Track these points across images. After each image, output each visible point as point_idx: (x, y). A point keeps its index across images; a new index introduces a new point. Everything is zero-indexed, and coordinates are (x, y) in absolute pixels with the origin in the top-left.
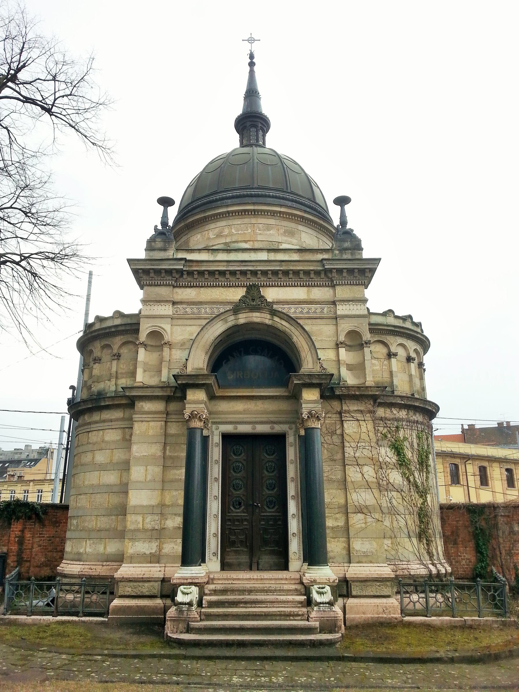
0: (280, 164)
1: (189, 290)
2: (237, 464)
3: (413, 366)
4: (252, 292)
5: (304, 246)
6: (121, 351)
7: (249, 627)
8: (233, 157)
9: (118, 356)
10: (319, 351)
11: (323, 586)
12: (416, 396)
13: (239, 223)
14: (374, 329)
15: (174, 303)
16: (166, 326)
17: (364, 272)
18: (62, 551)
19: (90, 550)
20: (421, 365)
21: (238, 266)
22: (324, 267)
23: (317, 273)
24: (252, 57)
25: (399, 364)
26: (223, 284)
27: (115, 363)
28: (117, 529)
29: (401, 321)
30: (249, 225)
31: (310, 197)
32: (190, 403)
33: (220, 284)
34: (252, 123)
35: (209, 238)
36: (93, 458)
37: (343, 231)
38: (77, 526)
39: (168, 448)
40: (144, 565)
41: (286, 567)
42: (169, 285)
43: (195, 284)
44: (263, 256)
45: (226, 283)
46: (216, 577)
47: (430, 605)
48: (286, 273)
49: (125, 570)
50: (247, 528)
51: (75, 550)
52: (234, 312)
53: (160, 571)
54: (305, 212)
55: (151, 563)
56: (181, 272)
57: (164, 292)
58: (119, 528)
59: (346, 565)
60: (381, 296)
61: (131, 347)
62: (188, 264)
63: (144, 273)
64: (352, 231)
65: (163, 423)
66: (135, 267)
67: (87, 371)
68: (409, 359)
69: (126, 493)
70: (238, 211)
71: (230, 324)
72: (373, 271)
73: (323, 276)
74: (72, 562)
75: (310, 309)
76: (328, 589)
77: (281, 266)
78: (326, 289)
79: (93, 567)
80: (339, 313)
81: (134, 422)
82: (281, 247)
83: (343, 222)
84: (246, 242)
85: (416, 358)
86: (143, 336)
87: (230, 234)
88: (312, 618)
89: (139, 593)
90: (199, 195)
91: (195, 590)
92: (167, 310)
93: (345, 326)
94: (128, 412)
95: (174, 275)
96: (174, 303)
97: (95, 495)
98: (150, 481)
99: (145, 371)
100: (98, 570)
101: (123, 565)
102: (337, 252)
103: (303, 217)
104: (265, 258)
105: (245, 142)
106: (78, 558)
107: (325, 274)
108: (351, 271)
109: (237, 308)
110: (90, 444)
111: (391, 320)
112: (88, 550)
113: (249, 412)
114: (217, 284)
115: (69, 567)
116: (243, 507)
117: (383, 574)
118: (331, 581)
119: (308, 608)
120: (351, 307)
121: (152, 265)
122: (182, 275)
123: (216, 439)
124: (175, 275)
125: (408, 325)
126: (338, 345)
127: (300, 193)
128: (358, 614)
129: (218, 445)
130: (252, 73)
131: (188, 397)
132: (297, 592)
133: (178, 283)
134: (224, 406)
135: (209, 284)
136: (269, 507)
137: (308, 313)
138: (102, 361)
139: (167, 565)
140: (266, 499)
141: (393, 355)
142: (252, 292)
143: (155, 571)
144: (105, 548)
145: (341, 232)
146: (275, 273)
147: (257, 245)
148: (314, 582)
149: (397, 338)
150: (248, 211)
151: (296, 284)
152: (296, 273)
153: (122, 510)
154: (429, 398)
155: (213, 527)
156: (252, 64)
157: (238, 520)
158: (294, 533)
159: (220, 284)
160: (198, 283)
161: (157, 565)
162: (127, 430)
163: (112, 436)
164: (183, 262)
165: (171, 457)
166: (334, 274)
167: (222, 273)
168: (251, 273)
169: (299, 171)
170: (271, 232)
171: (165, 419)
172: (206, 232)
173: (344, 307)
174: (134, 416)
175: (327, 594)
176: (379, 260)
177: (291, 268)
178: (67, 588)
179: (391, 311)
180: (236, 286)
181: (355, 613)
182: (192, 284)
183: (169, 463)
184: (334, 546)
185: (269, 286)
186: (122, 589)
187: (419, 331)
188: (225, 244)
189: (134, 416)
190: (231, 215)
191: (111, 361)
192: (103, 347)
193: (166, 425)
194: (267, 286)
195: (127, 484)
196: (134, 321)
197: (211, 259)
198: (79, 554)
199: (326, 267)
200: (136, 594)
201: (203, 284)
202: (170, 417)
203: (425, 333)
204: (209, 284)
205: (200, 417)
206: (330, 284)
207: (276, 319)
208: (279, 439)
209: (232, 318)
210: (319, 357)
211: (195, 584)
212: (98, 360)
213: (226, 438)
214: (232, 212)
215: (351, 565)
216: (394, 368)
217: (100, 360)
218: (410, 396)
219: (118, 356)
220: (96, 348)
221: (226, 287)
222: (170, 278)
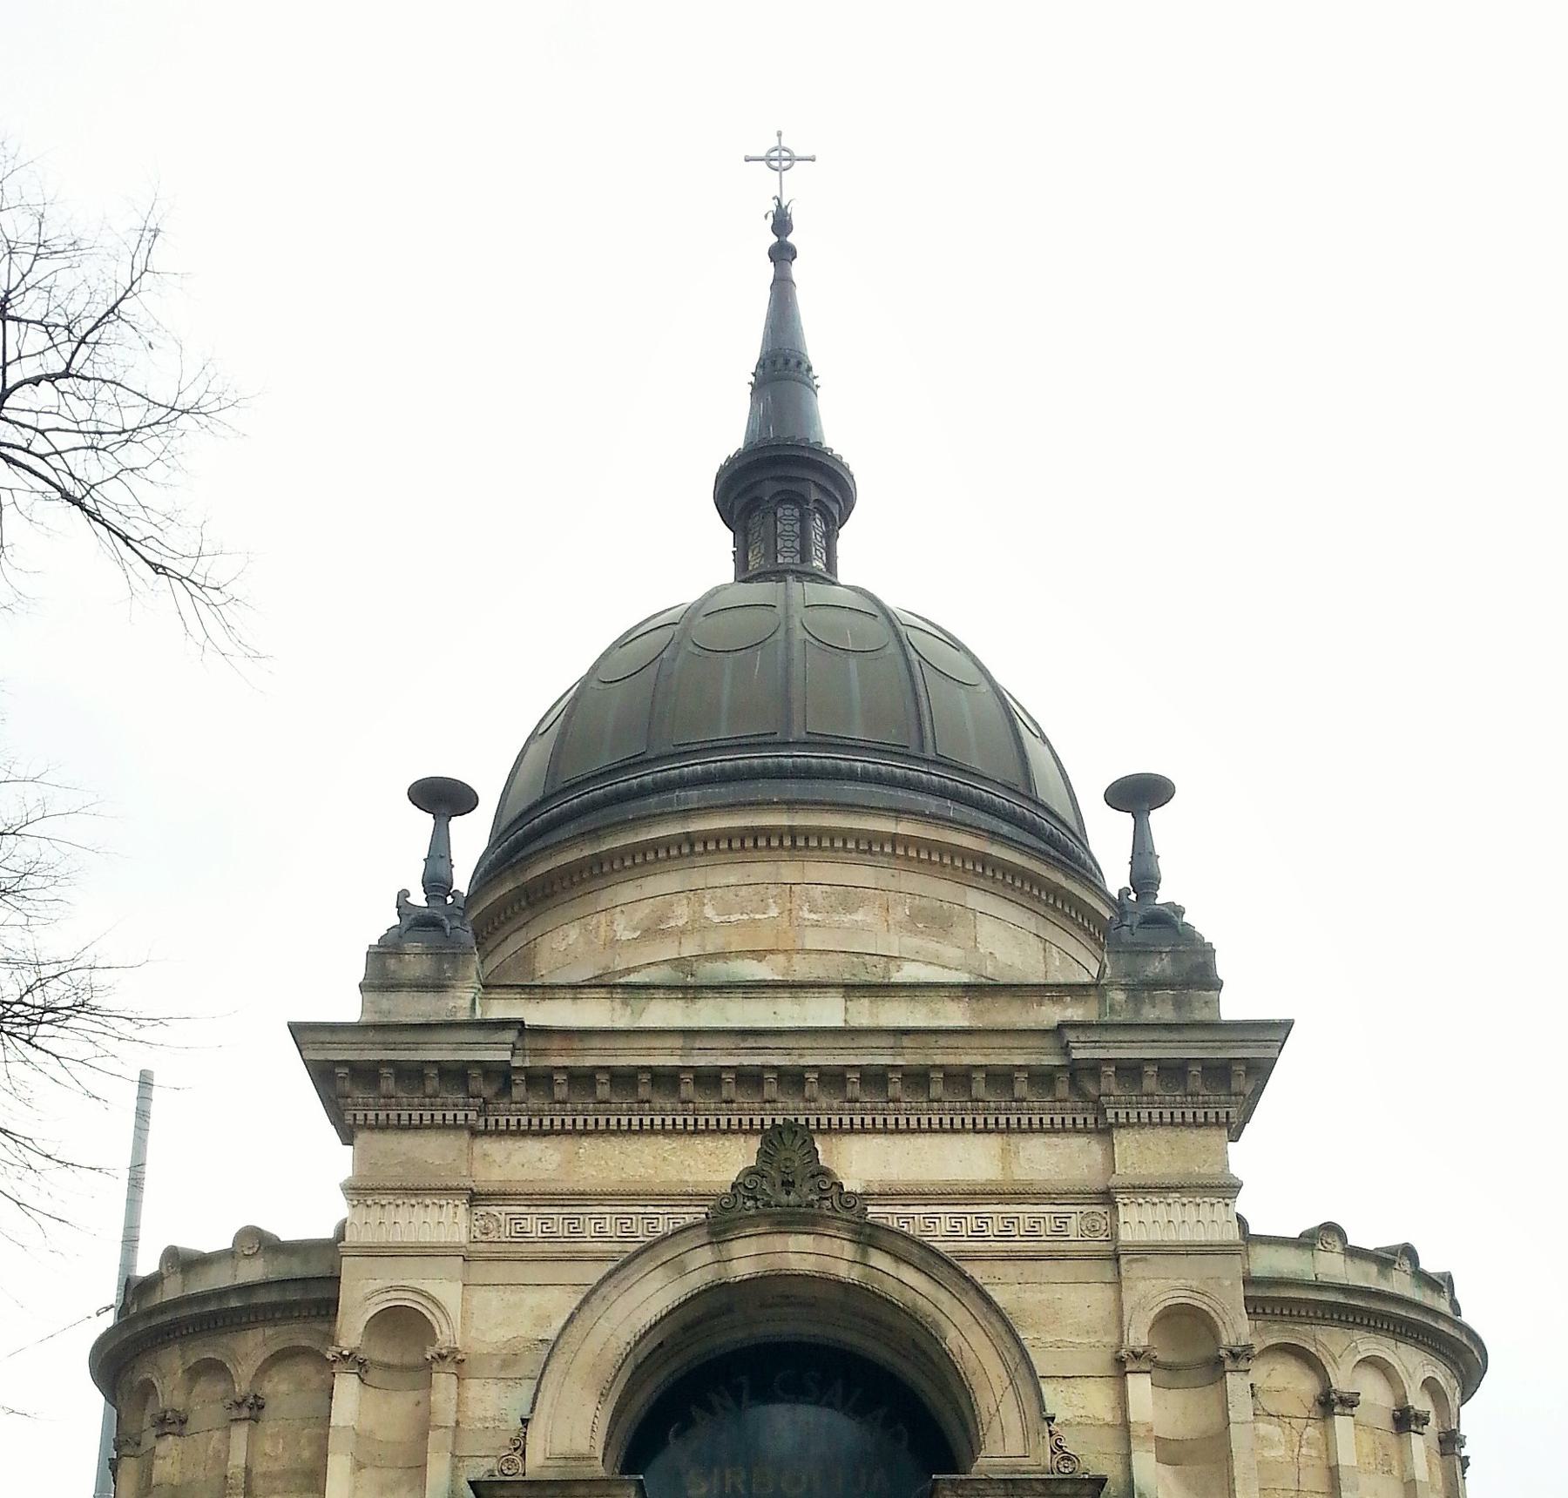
0: (893, 648)
3: (1420, 1446)
4: (784, 1154)
5: (990, 970)
6: (267, 1388)
7: (1042, 796)
8: (710, 620)
9: (253, 1408)
13: (732, 880)
14: (1266, 1300)
15: (475, 1198)
16: (444, 1289)
20: (1450, 1442)
22: (1068, 1054)
23: (1041, 1078)
24: (782, 223)
25: (1367, 1440)
26: (669, 1121)
27: (240, 1433)
29: (1373, 1269)
30: (773, 890)
31: (1014, 777)
34: (781, 487)
35: (613, 943)
42: (456, 1127)
44: (827, 1012)
48: (917, 1078)
52: (712, 1234)
54: (994, 836)
56: (501, 1075)
57: (434, 1152)
60: (1291, 1171)
61: (306, 1369)
62: (528, 1042)
64: (1180, 911)
66: (320, 1056)
67: (129, 1466)
68: (1405, 1420)
71: (697, 1280)
72: (1260, 1071)
73: (1062, 1089)
75: (1012, 1221)
77: (897, 1050)
78: (1078, 1142)
80: (1126, 1235)
82: (897, 977)
83: (1144, 876)
84: (759, 955)
85: (1432, 1417)
86: (351, 1329)
87: (698, 926)
90: (572, 773)
92: (448, 1224)
93: (1153, 1290)
96: (475, 1198)
99: (359, 1466)
102: (1120, 996)
103: (983, 859)
105: (754, 563)
107: (1074, 1083)
108: (1174, 1072)
109: (723, 1219)
111: (1331, 1266)
120: (1176, 1213)
121: (387, 1047)
122: (506, 1088)
124: (477, 1085)
125: (1399, 1283)
126: (1121, 1366)
127: (975, 764)
130: (782, 289)
135: (613, 1121)
137: (1004, 1236)
138: (192, 1425)
141: (1235, 1356)
142: (784, 1154)
145: (1137, 919)
147: (803, 970)
149: (1358, 1334)
150: (767, 832)
151: (958, 1121)
152: (959, 1078)
156: (782, 254)
160: (568, 1120)
164: (510, 1036)
167: (666, 1079)
168: (779, 1080)
169: (971, 676)
170: (859, 916)
172: (603, 917)
173: (1148, 1213)
176: (1286, 1026)
177: (939, 1059)
179: (1331, 1229)
182: (546, 1122)
188: (678, 963)
191: (228, 1428)
192: (197, 1372)
196: (316, 1269)
197: (622, 1023)
199: (1076, 1055)
201: (591, 1120)
204: (613, 1121)
206: (1091, 1120)
207: (879, 1260)
209: (706, 1255)
210: (1049, 1411)
214: (705, 838)
216: (1346, 1456)
217: (183, 1422)
219: (253, 1408)
220: (168, 1376)
221: (680, 1133)
222: (459, 1097)
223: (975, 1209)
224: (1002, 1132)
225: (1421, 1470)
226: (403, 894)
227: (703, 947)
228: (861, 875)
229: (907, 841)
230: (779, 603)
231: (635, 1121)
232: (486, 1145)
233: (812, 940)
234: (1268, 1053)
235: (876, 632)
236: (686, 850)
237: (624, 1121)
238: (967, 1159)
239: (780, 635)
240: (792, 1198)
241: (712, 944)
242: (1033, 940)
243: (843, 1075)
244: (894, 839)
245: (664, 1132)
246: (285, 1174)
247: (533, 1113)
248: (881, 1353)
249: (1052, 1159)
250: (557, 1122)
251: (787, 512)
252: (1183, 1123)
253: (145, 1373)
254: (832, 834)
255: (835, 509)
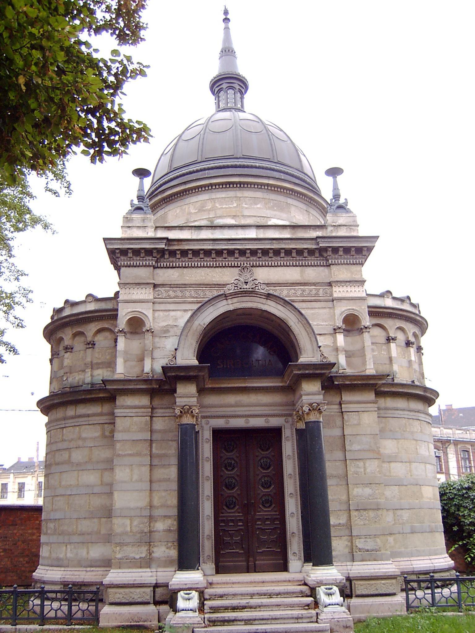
0: (264, 131)
1: (170, 271)
2: (229, 461)
3: (412, 350)
4: (246, 274)
5: (294, 221)
6: (96, 339)
7: (305, 172)
9: (92, 345)
10: (318, 337)
11: (330, 587)
12: (417, 383)
13: (223, 196)
14: (375, 312)
16: (147, 311)
17: (357, 250)
18: (38, 556)
19: (71, 555)
20: (419, 349)
21: (225, 245)
22: (318, 245)
23: (311, 252)
24: (226, 12)
25: (399, 349)
26: (208, 264)
27: (89, 351)
28: (100, 533)
29: (400, 302)
30: (235, 199)
31: (299, 167)
32: (180, 397)
33: (205, 264)
34: (229, 84)
35: (190, 213)
36: (70, 457)
37: (337, 205)
38: (55, 530)
39: (154, 445)
40: (134, 570)
41: (284, 568)
42: (149, 266)
43: (177, 264)
44: (252, 234)
45: (211, 264)
46: (214, 582)
47: (436, 602)
48: (277, 252)
49: (114, 576)
50: (242, 529)
51: (54, 555)
53: (152, 576)
54: (295, 184)
55: (141, 567)
56: (162, 252)
57: (143, 273)
58: (103, 531)
59: (348, 563)
60: (378, 277)
61: (107, 334)
63: (120, 254)
65: (148, 418)
66: (111, 247)
67: (55, 361)
68: (408, 344)
69: (110, 494)
70: (222, 184)
72: (370, 249)
74: (51, 568)
75: (304, 291)
76: (336, 589)
78: (322, 268)
79: (76, 573)
80: (335, 295)
81: (116, 418)
82: (270, 223)
85: (415, 343)
86: (122, 322)
88: (322, 620)
89: (131, 600)
90: (175, 165)
91: (195, 595)
92: (146, 294)
93: (341, 310)
94: (106, 408)
95: (154, 255)
96: (155, 286)
97: (73, 496)
98: (136, 481)
99: (125, 361)
100: (82, 577)
101: (112, 571)
103: (292, 190)
104: (254, 236)
105: (222, 105)
106: (58, 564)
107: (320, 252)
110: (65, 441)
111: (389, 303)
112: (69, 555)
113: (249, 407)
114: (202, 264)
115: (44, 573)
116: (237, 507)
117: (388, 572)
118: (338, 582)
119: (316, 610)
120: (349, 289)
122: (163, 256)
123: (206, 435)
125: (406, 307)
126: (336, 330)
128: (363, 613)
129: (207, 441)
131: (178, 390)
132: (303, 595)
133: (159, 264)
134: (212, 400)
135: (193, 264)
136: (264, 506)
137: (302, 295)
138: (74, 350)
139: (160, 569)
140: (261, 498)
141: (393, 339)
142: (246, 274)
143: (148, 576)
144: (88, 553)
145: (335, 207)
146: (265, 252)
147: (243, 222)
148: (320, 583)
149: (396, 320)
150: (233, 183)
151: (288, 263)
152: (288, 252)
153: (108, 513)
154: (428, 384)
155: (207, 527)
156: (226, 20)
157: (232, 521)
158: (293, 533)
159: (205, 264)
160: (181, 264)
161: (148, 570)
162: (106, 425)
163: (91, 433)
165: (160, 456)
166: (329, 253)
167: (207, 253)
168: (239, 253)
169: (285, 138)
170: (259, 206)
171: (150, 414)
172: (187, 206)
173: (341, 289)
174: (116, 411)
175: (335, 595)
176: (378, 237)
178: (54, 595)
179: (389, 292)
180: (222, 267)
181: (360, 613)
182: (174, 264)
183: (155, 462)
184: (338, 545)
185: (259, 266)
186: (114, 595)
187: (417, 312)
188: (208, 219)
189: (116, 411)
190: (214, 187)
191: (86, 350)
192: (75, 335)
193: (151, 420)
194: (256, 266)
195: (111, 485)
196: (109, 306)
197: (194, 237)
198: (58, 559)
199: (321, 245)
200: (127, 601)
201: (187, 264)
202: (155, 411)
203: (421, 315)
204: (193, 264)
205: (192, 412)
206: (325, 263)
208: (275, 434)
210: (320, 344)
211: (196, 589)
212: (69, 349)
213: (217, 433)
214: (215, 184)
215: (355, 563)
216: (394, 353)
217: (72, 349)
218: (410, 383)
219: (92, 345)
220: (67, 335)
221: (212, 267)
222: (150, 258)
223: (294, 288)
224: (300, 266)
225: (413, 358)
226: (132, 201)
227: (216, 214)
228: (259, 194)
229: (272, 185)
230: (233, 118)
231: (199, 264)
232: (158, 271)
233: (246, 213)
234: (373, 245)
235: (259, 127)
236: (210, 188)
237: (196, 264)
238: (291, 274)
239: (233, 128)
240: (247, 287)
241: (219, 213)
242: (305, 212)
243: (257, 251)
244: (268, 185)
245: (207, 267)
246: (103, 281)
247: (170, 262)
248: (269, 328)
249: (313, 274)
250: (177, 264)
251: (231, 92)
252: (350, 264)
253: (60, 335)
254: (251, 183)
255: (243, 91)
